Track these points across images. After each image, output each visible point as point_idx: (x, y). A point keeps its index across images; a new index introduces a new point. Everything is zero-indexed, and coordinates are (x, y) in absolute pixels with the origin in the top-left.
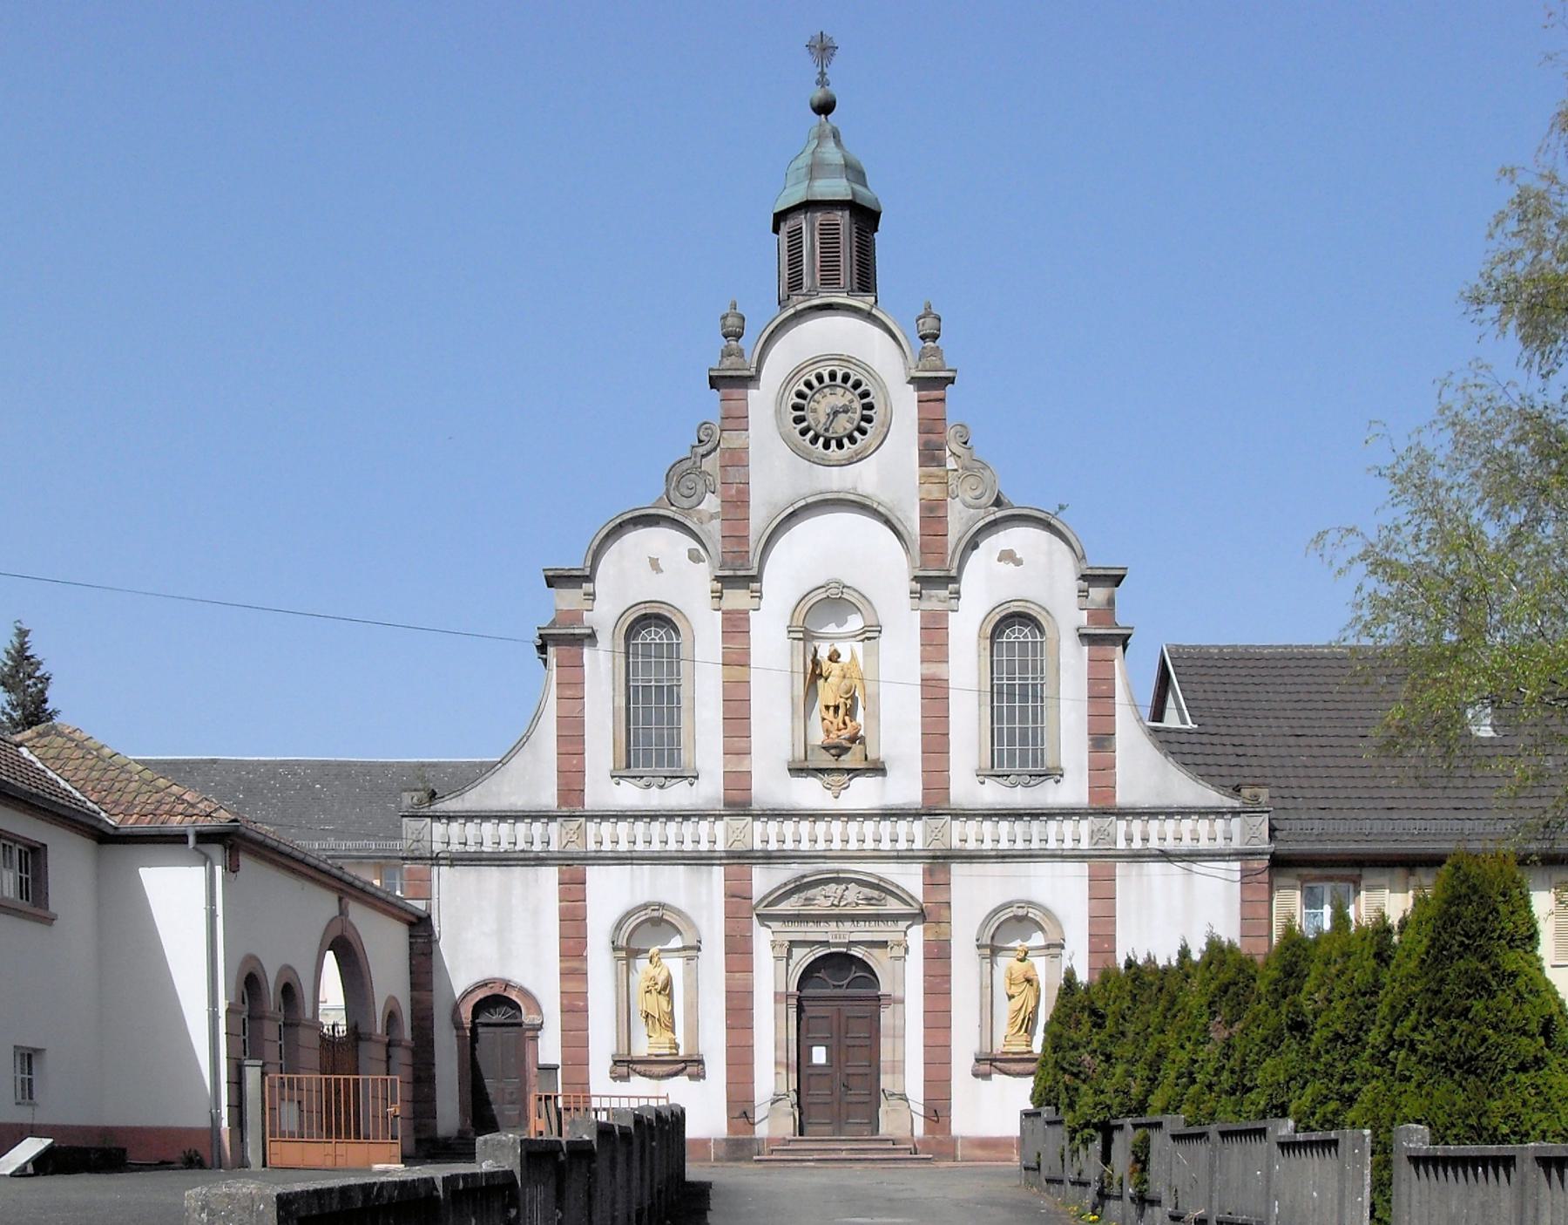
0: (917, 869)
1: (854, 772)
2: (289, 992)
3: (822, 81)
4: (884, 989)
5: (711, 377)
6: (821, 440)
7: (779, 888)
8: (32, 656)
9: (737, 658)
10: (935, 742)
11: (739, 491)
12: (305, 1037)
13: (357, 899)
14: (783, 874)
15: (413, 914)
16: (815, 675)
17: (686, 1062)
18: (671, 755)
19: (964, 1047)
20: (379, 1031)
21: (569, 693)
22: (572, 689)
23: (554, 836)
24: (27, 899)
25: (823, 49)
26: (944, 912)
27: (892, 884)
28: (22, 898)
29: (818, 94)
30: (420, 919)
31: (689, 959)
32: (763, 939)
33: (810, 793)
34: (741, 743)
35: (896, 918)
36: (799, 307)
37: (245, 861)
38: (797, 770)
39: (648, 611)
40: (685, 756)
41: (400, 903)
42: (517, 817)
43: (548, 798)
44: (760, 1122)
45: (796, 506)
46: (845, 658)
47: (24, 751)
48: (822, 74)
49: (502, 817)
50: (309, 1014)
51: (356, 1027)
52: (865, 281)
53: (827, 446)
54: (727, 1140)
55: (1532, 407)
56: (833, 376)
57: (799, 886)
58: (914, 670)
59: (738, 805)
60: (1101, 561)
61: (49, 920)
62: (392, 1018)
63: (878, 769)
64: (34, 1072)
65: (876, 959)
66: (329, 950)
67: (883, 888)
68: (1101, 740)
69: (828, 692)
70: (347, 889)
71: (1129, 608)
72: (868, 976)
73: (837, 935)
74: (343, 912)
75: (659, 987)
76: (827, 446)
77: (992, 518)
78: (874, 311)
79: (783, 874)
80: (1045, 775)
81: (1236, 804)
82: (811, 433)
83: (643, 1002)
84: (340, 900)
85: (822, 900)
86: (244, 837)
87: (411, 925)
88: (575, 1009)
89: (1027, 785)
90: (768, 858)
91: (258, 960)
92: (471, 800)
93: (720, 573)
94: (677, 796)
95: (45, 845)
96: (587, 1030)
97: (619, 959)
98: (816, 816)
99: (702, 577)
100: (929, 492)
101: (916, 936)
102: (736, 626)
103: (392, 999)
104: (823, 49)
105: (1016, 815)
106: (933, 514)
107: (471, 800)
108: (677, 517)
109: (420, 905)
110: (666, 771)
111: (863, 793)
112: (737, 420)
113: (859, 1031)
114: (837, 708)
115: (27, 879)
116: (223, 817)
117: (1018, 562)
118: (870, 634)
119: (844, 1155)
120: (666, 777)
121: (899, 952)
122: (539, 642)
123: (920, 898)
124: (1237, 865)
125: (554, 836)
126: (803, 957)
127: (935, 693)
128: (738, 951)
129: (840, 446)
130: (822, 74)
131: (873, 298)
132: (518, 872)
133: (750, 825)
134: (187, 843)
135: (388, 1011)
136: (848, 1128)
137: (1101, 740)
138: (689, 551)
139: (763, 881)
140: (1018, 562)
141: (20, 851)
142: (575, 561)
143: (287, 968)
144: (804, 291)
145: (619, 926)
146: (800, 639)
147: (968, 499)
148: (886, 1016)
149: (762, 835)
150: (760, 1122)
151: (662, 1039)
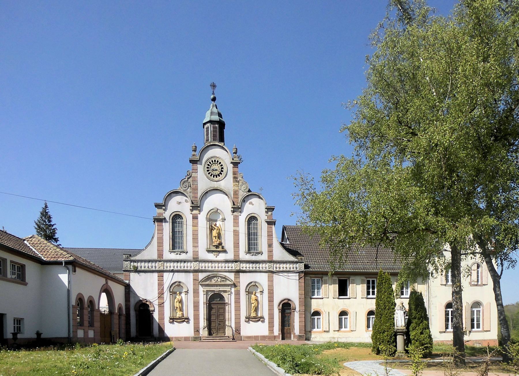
0: (233, 274)
1: (219, 252)
2: (91, 302)
3: (213, 94)
4: (226, 301)
5: (190, 160)
6: (213, 175)
7: (204, 278)
8: (38, 220)
9: (195, 225)
10: (236, 245)
11: (196, 187)
12: (95, 313)
13: (110, 280)
14: (205, 275)
15: (126, 284)
16: (211, 229)
17: (186, 319)
18: (181, 247)
19: (243, 314)
20: (116, 312)
21: (160, 232)
22: (161, 231)
23: (158, 266)
24: (20, 279)
25: (214, 86)
26: (238, 284)
27: (228, 277)
28: (18, 278)
29: (216, 102)
30: (127, 285)
31: (186, 294)
32: (201, 289)
33: (211, 257)
34: (196, 244)
35: (228, 285)
36: (208, 145)
37: (77, 269)
38: (209, 251)
39: (177, 213)
40: (185, 247)
41: (122, 281)
42: (149, 261)
43: (155, 257)
44: (502, 273)
45: (208, 190)
46: (218, 225)
47: (25, 242)
48: (213, 92)
49: (145, 261)
50: (97, 308)
51: (111, 311)
52: (222, 139)
53: (214, 177)
54: (194, 337)
55: (396, 32)
56: (215, 161)
57: (208, 278)
58: (232, 228)
59: (196, 260)
60: (271, 205)
61: (26, 284)
62: (120, 309)
63: (225, 251)
64: (21, 324)
65: (225, 295)
66: (103, 292)
67: (225, 278)
68: (270, 245)
69: (215, 233)
70: (108, 277)
71: (275, 215)
72: (222, 298)
73: (216, 289)
74: (107, 283)
75: (179, 301)
76: (214, 177)
77: (248, 194)
78: (224, 146)
79: (205, 275)
80: (259, 253)
81: (296, 260)
82: (211, 174)
83: (177, 305)
84: (106, 280)
85: (213, 282)
86: (77, 263)
87: (125, 286)
88: (161, 305)
89: (255, 255)
90: (202, 271)
91: (82, 294)
92: (138, 257)
93: (192, 205)
94: (183, 256)
95: (25, 265)
96: (164, 311)
97: (171, 294)
98: (212, 262)
99: (188, 205)
100: (235, 188)
101: (233, 290)
102: (195, 218)
103: (120, 304)
104: (214, 86)
105: (253, 262)
106: (236, 193)
107: (138, 257)
108: (182, 192)
109: (127, 282)
110: (180, 250)
111: (222, 257)
112: (196, 171)
113: (221, 311)
114: (216, 237)
115: (20, 274)
116: (71, 258)
117: (253, 205)
118: (224, 220)
119: (218, 340)
120: (180, 252)
121: (229, 293)
122: (153, 220)
123: (234, 280)
124: (298, 274)
125: (158, 266)
126: (210, 294)
127: (236, 234)
128: (196, 292)
129: (217, 177)
130: (213, 92)
131: (223, 144)
132: (149, 274)
133: (198, 264)
134: (63, 265)
135: (119, 307)
136: (219, 334)
137: (270, 245)
138: (185, 200)
139: (201, 276)
140: (253, 205)
141: (18, 266)
142: (161, 201)
143: (90, 297)
144: (209, 141)
145: (279, 306)
146: (208, 221)
147: (243, 190)
148: (227, 308)
149: (203, 266)
150: (502, 273)
151: (180, 313)
